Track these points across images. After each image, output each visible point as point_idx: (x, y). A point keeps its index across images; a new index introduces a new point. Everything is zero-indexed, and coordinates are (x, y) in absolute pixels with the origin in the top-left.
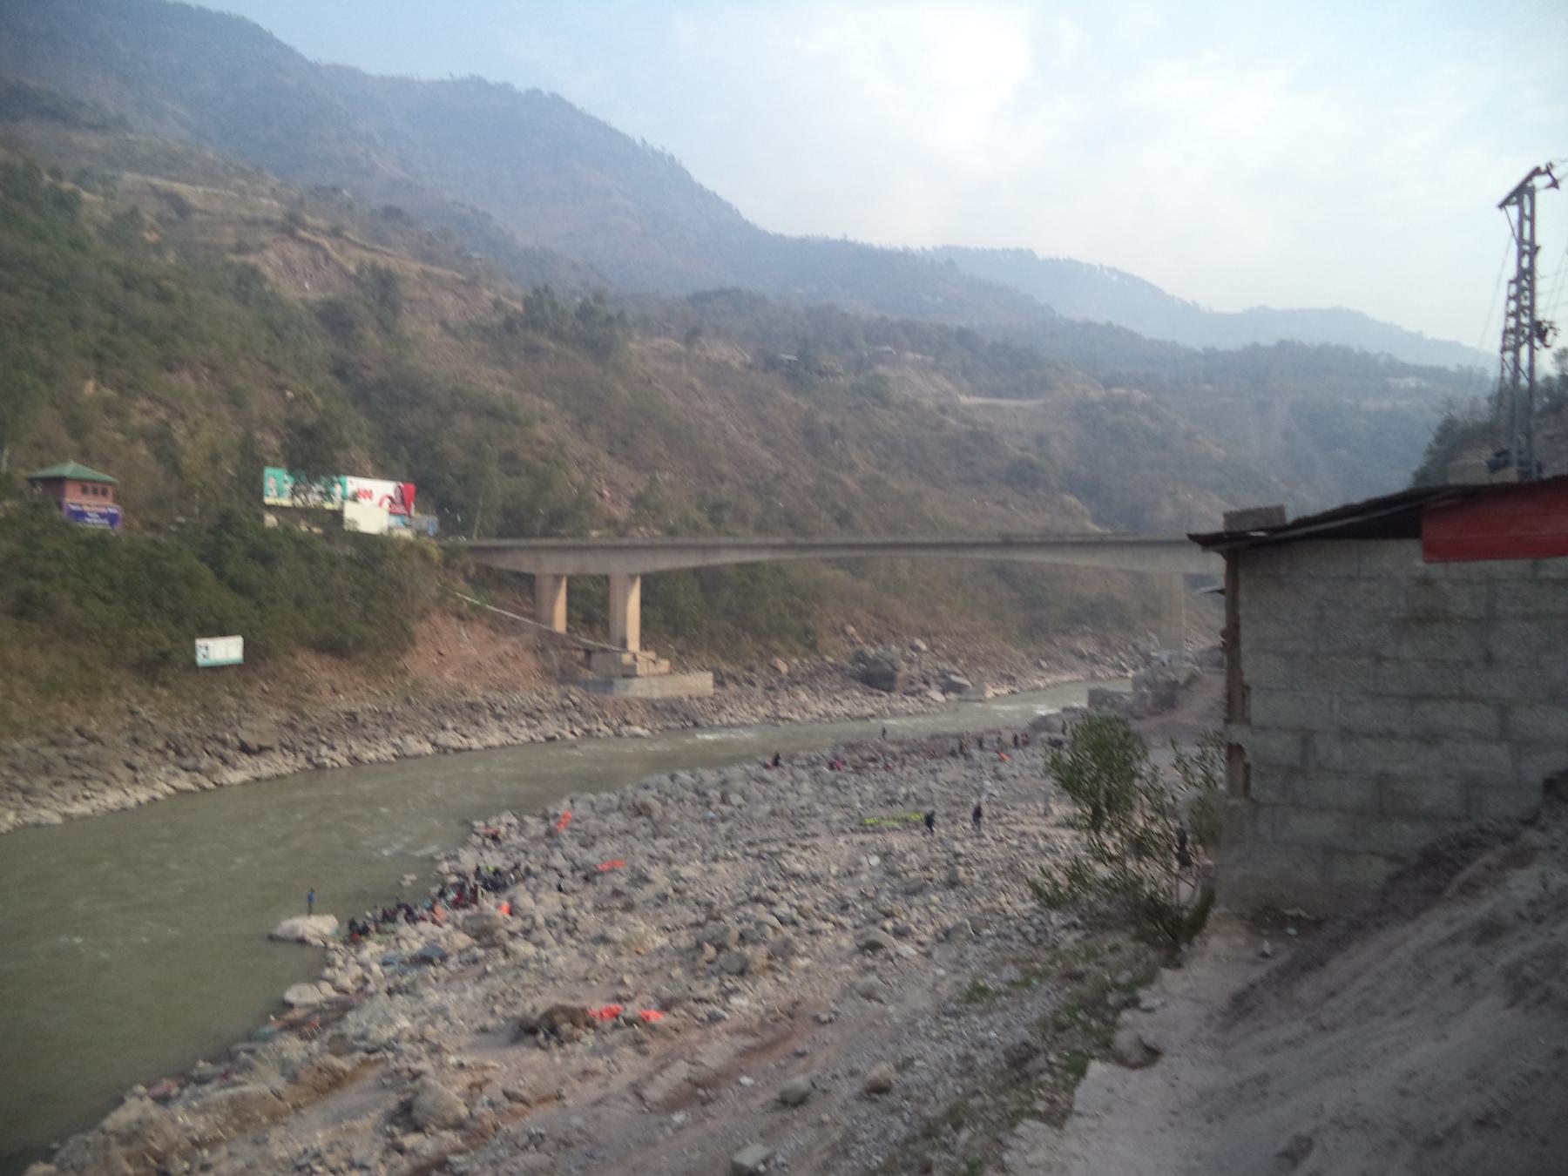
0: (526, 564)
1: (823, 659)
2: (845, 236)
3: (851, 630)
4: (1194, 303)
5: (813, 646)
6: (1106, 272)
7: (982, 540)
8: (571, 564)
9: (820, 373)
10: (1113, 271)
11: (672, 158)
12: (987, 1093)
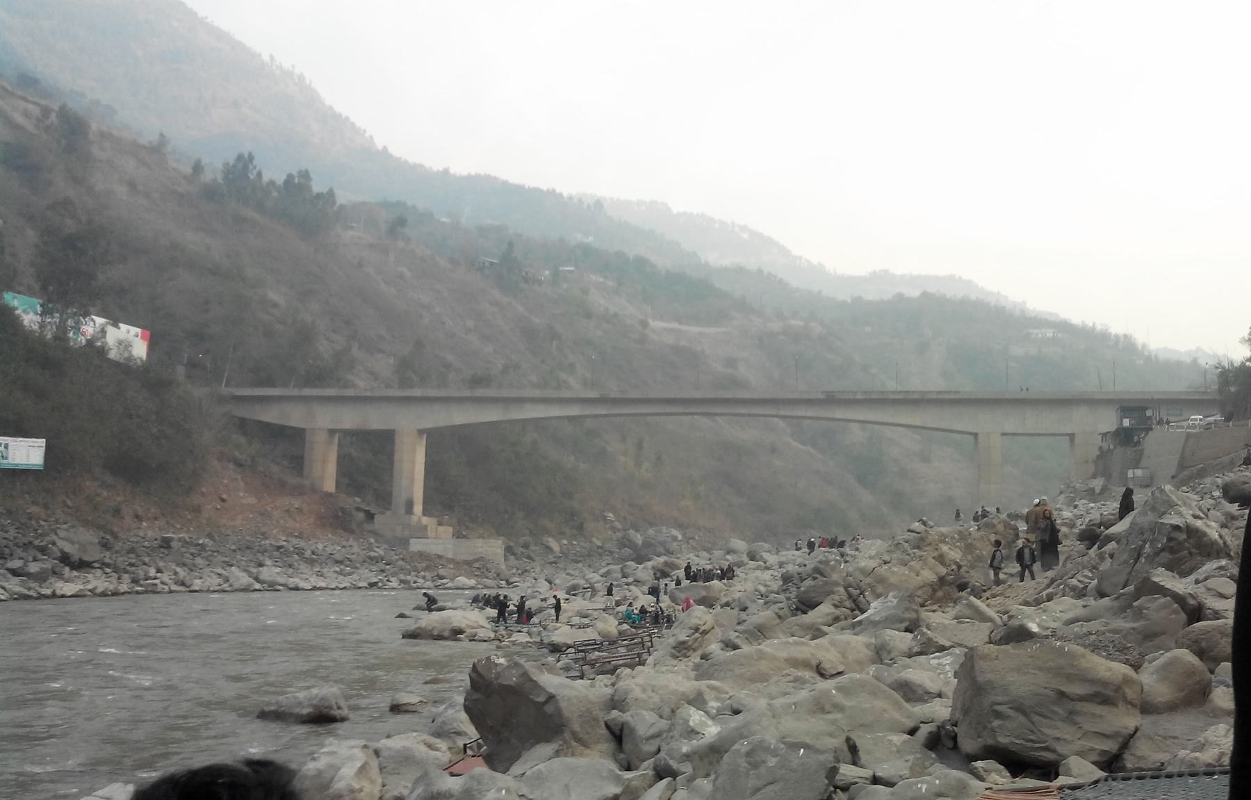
0: (294, 417)
1: (591, 542)
2: (449, 168)
3: (611, 516)
4: (819, 264)
5: (580, 528)
6: (737, 229)
7: (805, 396)
8: (349, 419)
9: (526, 280)
10: (744, 228)
11: (301, 78)
12: (1083, 656)
